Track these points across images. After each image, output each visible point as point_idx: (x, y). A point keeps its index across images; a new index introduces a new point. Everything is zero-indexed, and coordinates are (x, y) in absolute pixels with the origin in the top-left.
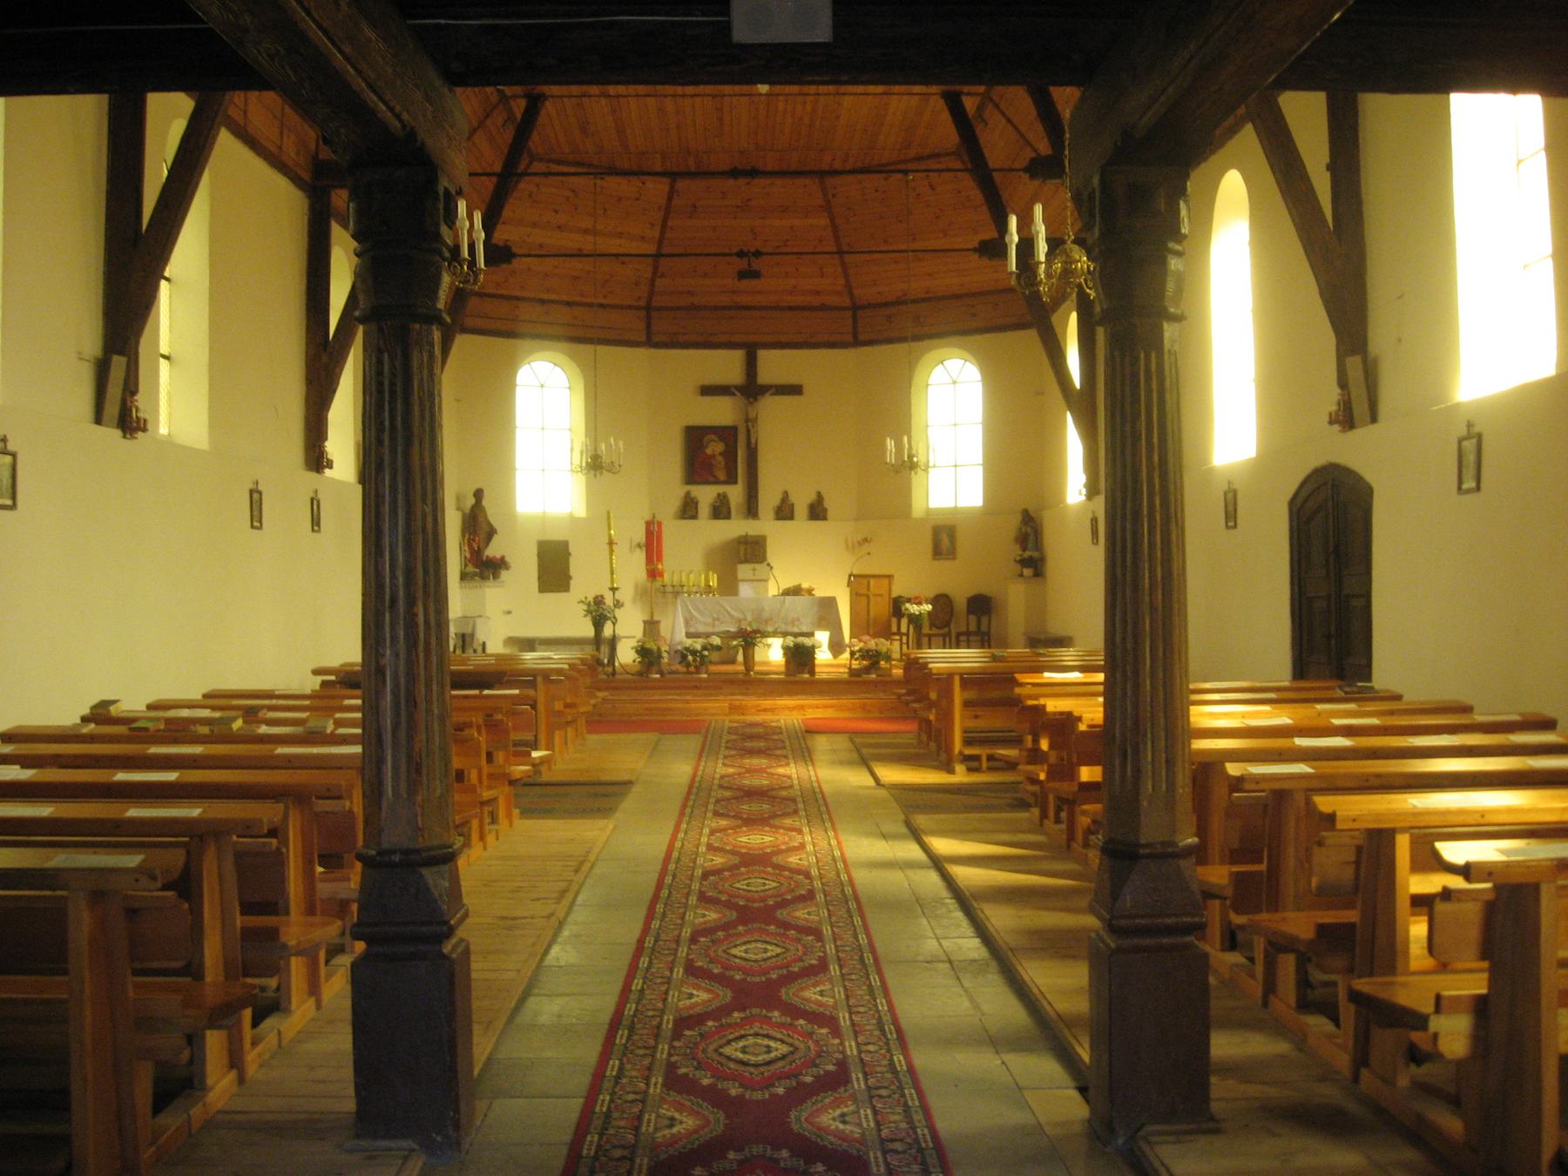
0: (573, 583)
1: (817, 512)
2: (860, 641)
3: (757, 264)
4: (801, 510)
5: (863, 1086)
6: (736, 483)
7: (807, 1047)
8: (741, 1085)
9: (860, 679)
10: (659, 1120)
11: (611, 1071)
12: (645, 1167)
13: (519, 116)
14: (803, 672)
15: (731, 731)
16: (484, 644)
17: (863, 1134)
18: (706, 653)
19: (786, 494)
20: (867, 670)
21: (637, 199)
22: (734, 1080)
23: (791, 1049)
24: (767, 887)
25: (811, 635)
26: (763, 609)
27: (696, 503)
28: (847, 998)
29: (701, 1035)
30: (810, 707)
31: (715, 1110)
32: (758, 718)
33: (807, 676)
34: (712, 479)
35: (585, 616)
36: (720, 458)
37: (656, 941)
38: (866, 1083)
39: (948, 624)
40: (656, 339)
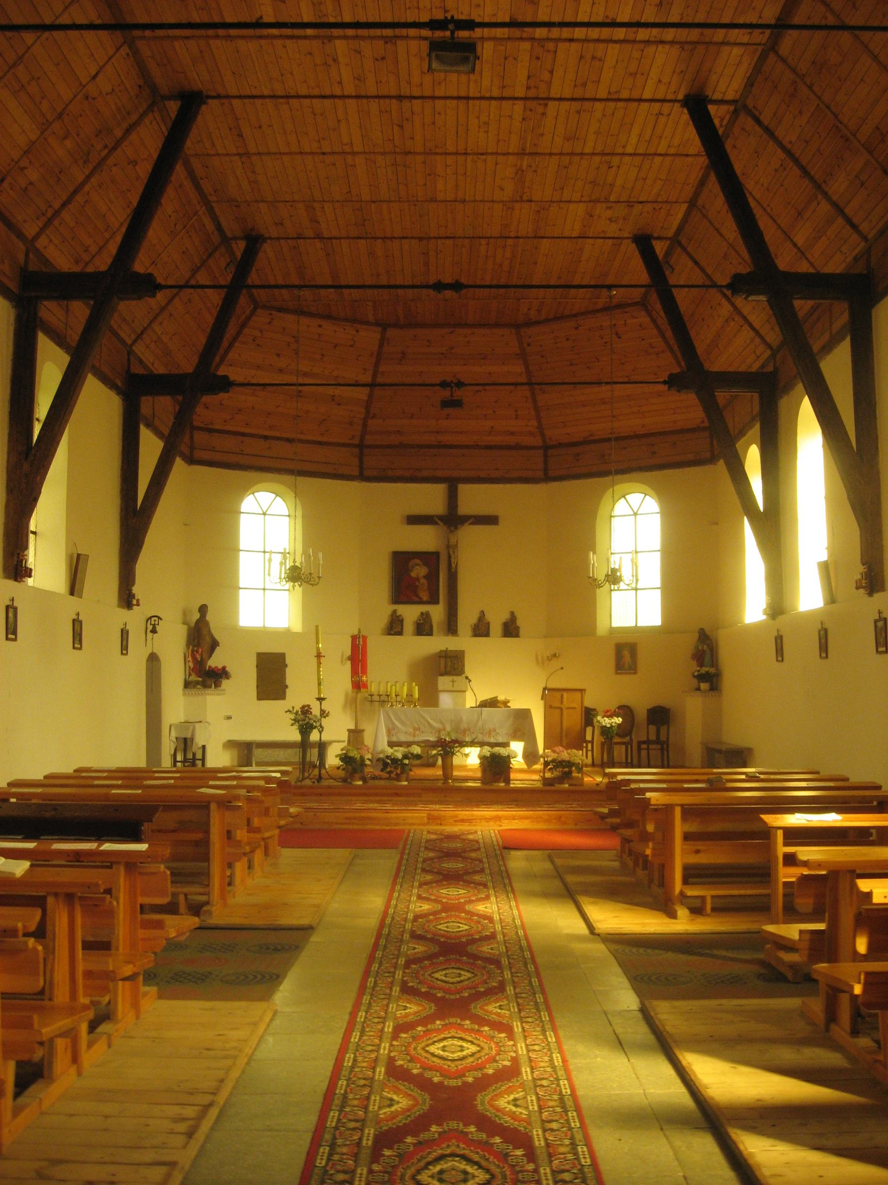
0: (288, 692)
1: (510, 630)
2: (554, 752)
3: (459, 393)
4: (496, 628)
7: (490, 1048)
8: (441, 1075)
9: (553, 788)
12: (372, 1135)
13: (239, 255)
14: (498, 781)
15: (430, 845)
16: (204, 747)
17: (529, 1115)
18: (406, 761)
19: (482, 613)
20: (560, 780)
21: (351, 346)
22: (437, 1071)
23: (478, 1049)
24: (461, 929)
25: (505, 745)
26: (461, 720)
27: (402, 621)
28: (499, 910)
29: (400, 1156)
30: (507, 818)
31: (423, 1093)
32: (456, 829)
33: (502, 784)
34: (417, 599)
35: (292, 725)
38: (532, 1076)
39: (629, 733)
40: (367, 473)
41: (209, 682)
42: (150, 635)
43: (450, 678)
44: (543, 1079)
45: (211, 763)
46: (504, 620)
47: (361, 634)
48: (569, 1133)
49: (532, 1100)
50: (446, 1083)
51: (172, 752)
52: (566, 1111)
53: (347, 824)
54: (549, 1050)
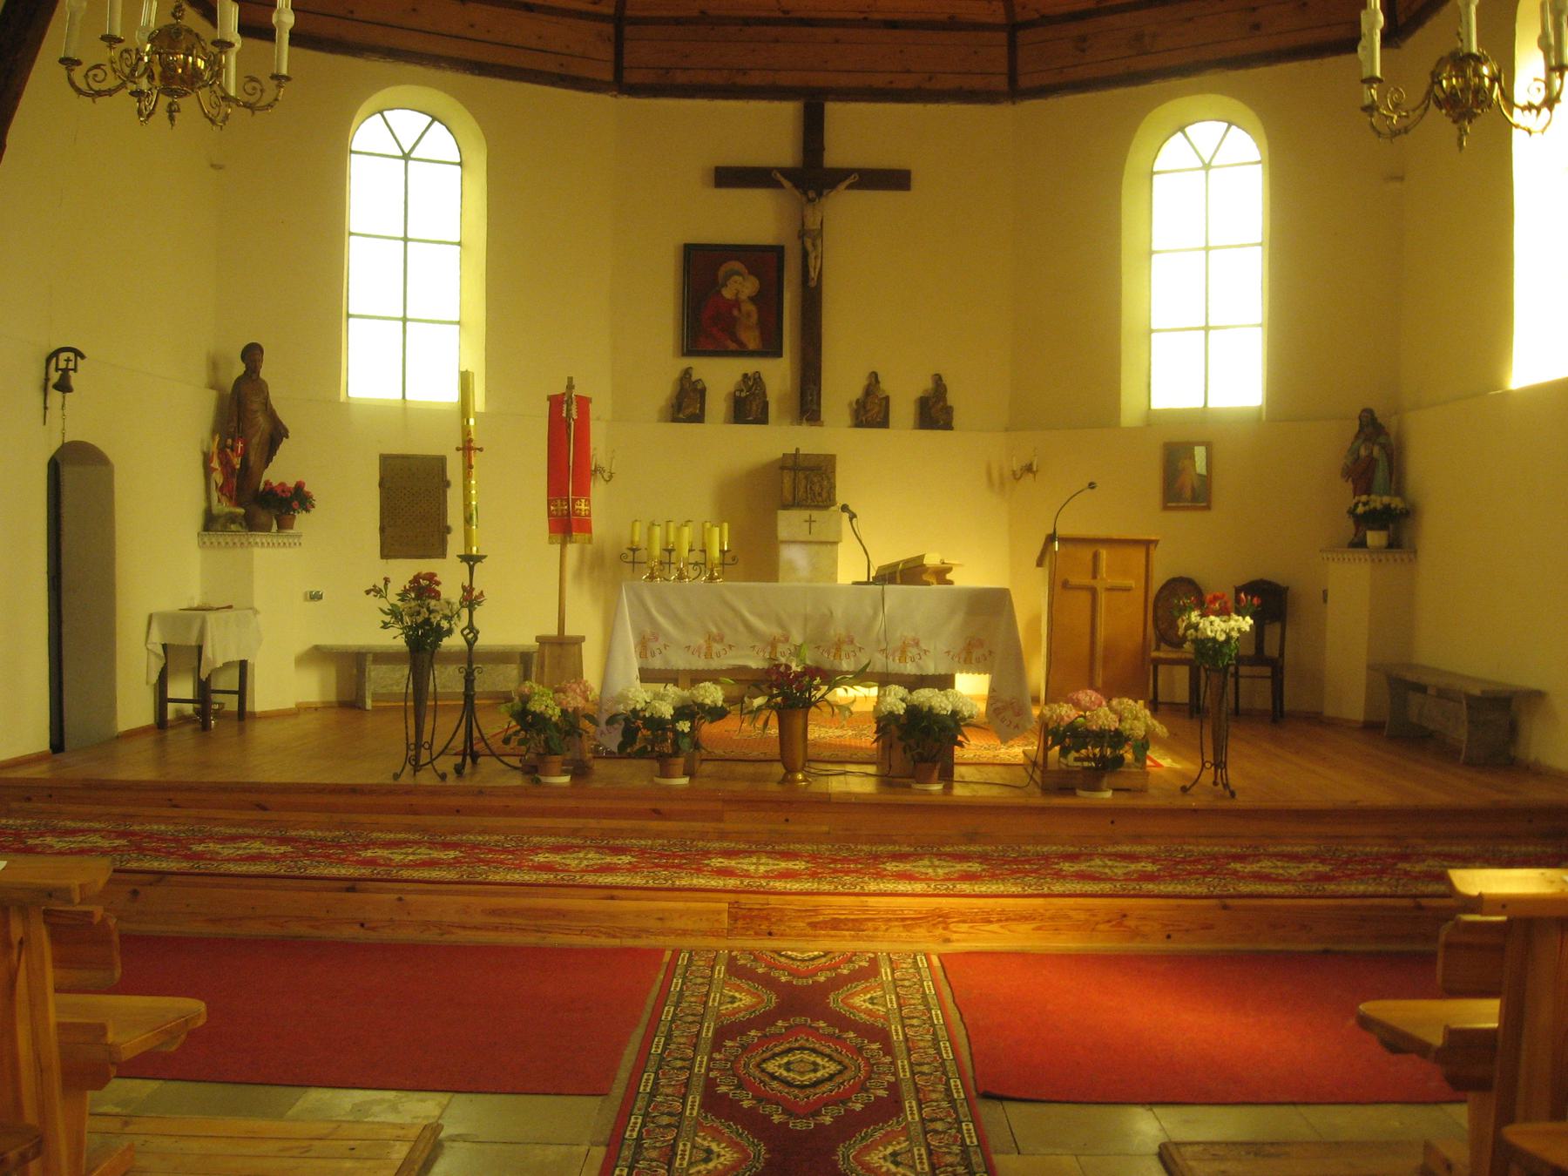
4: (903, 409)
5: (917, 1117)
6: (777, 353)
10: (695, 1151)
11: (645, 1087)
17: (887, 1012)
18: (684, 726)
19: (874, 377)
22: (777, 1104)
25: (945, 682)
26: (828, 618)
27: (703, 392)
28: (900, 1006)
30: (965, 917)
34: (733, 346)
36: (749, 307)
37: (666, 1044)
38: (920, 1114)
40: (632, 77)
41: (262, 517)
42: (55, 396)
43: (805, 514)
44: (913, 1018)
45: (263, 699)
46: (919, 394)
47: (575, 392)
48: (921, 989)
49: (920, 1155)
50: (794, 983)
51: (154, 678)
52: (929, 1010)
53: (496, 928)
54: (945, 1073)
